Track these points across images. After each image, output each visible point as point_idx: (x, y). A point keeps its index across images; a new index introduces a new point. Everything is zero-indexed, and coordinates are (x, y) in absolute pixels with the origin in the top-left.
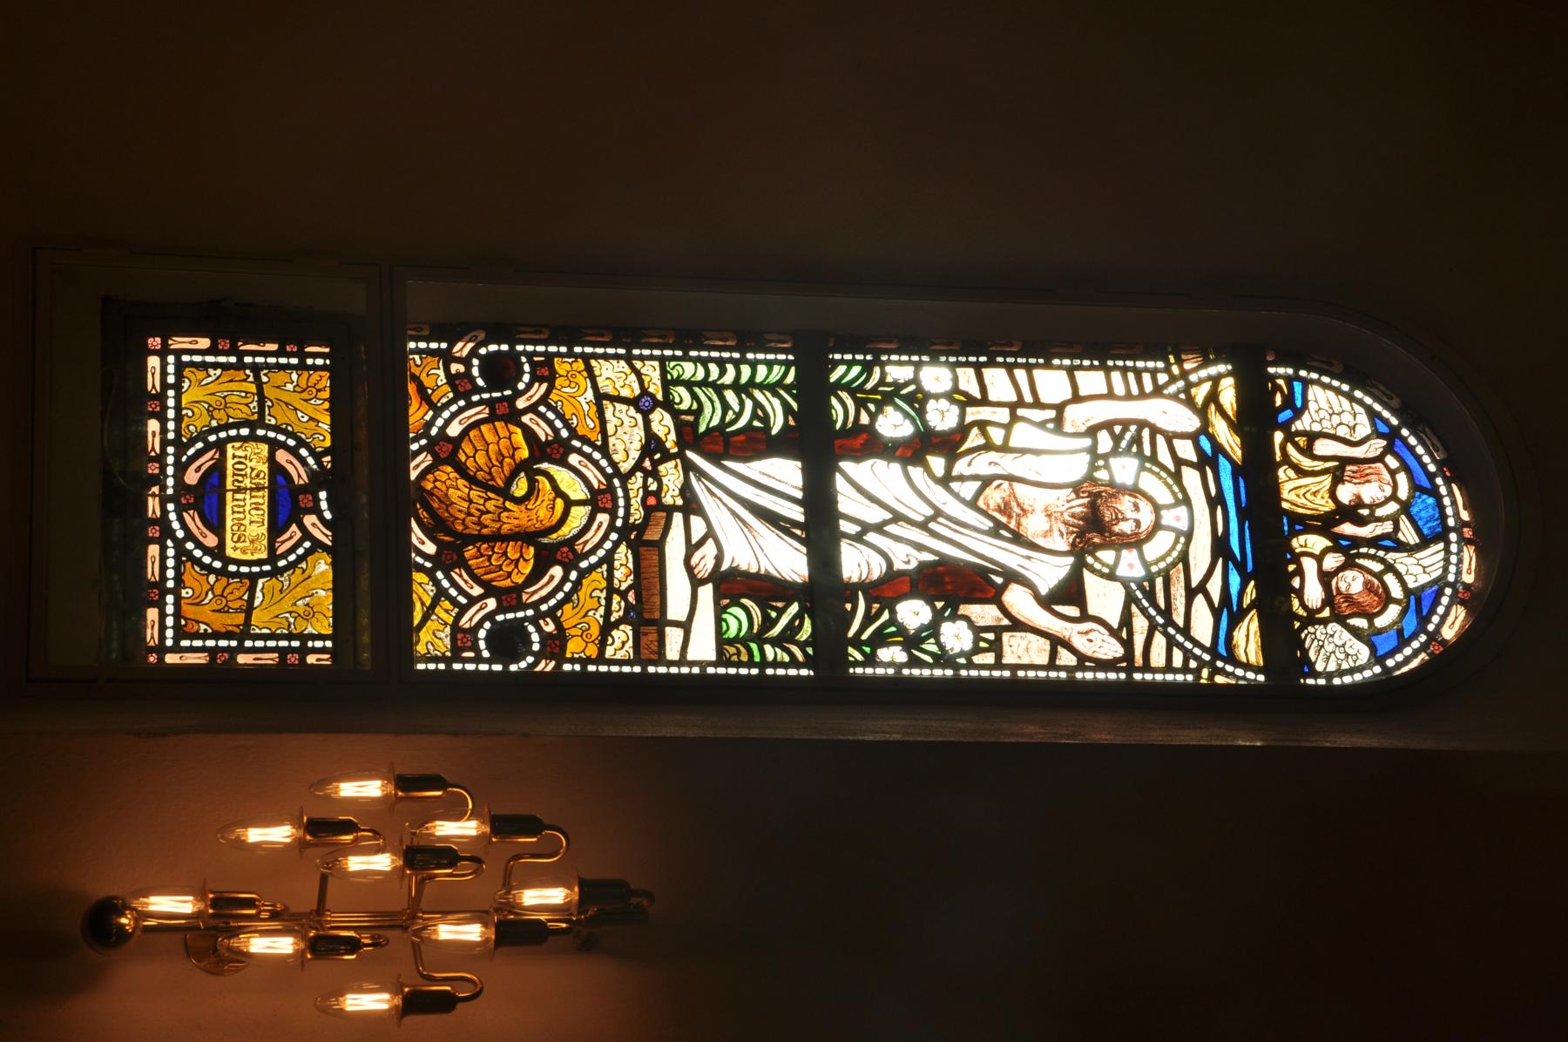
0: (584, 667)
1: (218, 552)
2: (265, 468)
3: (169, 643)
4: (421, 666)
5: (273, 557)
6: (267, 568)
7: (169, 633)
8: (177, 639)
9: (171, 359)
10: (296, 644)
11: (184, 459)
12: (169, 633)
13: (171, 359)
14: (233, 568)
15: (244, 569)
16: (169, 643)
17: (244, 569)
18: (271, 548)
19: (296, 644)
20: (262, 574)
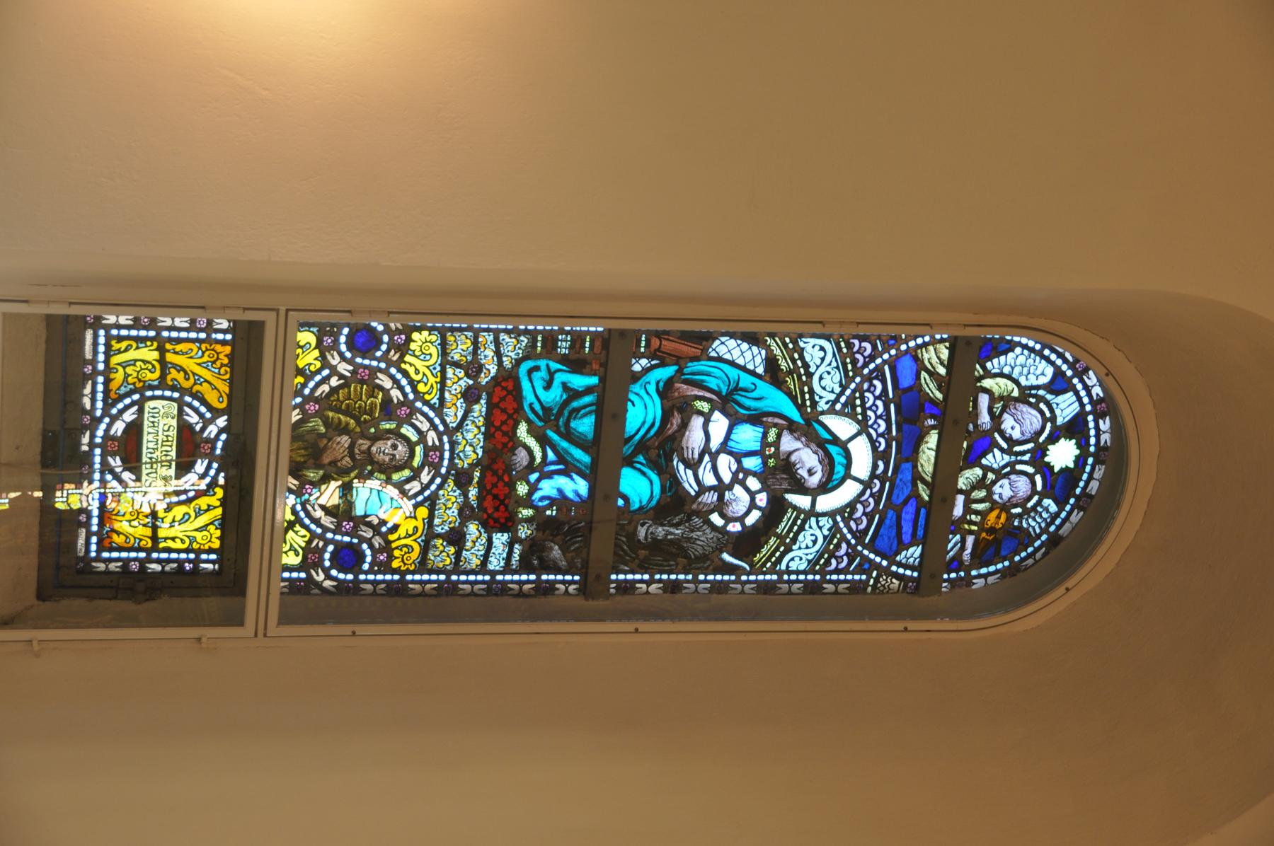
0: (932, 337)
1: (181, 404)
2: (174, 423)
3: (93, 554)
4: (577, 578)
5: (140, 404)
6: (149, 393)
7: (94, 547)
8: (99, 551)
9: (102, 332)
10: (192, 556)
11: (860, 417)
12: (94, 547)
13: (102, 332)
14: (176, 395)
15: (168, 393)
16: (93, 554)
17: (168, 393)
18: (141, 411)
19: (192, 556)
20: (152, 388)
